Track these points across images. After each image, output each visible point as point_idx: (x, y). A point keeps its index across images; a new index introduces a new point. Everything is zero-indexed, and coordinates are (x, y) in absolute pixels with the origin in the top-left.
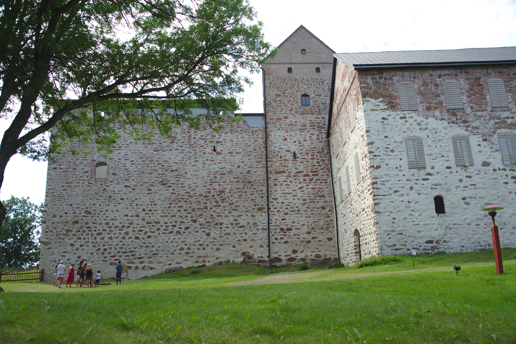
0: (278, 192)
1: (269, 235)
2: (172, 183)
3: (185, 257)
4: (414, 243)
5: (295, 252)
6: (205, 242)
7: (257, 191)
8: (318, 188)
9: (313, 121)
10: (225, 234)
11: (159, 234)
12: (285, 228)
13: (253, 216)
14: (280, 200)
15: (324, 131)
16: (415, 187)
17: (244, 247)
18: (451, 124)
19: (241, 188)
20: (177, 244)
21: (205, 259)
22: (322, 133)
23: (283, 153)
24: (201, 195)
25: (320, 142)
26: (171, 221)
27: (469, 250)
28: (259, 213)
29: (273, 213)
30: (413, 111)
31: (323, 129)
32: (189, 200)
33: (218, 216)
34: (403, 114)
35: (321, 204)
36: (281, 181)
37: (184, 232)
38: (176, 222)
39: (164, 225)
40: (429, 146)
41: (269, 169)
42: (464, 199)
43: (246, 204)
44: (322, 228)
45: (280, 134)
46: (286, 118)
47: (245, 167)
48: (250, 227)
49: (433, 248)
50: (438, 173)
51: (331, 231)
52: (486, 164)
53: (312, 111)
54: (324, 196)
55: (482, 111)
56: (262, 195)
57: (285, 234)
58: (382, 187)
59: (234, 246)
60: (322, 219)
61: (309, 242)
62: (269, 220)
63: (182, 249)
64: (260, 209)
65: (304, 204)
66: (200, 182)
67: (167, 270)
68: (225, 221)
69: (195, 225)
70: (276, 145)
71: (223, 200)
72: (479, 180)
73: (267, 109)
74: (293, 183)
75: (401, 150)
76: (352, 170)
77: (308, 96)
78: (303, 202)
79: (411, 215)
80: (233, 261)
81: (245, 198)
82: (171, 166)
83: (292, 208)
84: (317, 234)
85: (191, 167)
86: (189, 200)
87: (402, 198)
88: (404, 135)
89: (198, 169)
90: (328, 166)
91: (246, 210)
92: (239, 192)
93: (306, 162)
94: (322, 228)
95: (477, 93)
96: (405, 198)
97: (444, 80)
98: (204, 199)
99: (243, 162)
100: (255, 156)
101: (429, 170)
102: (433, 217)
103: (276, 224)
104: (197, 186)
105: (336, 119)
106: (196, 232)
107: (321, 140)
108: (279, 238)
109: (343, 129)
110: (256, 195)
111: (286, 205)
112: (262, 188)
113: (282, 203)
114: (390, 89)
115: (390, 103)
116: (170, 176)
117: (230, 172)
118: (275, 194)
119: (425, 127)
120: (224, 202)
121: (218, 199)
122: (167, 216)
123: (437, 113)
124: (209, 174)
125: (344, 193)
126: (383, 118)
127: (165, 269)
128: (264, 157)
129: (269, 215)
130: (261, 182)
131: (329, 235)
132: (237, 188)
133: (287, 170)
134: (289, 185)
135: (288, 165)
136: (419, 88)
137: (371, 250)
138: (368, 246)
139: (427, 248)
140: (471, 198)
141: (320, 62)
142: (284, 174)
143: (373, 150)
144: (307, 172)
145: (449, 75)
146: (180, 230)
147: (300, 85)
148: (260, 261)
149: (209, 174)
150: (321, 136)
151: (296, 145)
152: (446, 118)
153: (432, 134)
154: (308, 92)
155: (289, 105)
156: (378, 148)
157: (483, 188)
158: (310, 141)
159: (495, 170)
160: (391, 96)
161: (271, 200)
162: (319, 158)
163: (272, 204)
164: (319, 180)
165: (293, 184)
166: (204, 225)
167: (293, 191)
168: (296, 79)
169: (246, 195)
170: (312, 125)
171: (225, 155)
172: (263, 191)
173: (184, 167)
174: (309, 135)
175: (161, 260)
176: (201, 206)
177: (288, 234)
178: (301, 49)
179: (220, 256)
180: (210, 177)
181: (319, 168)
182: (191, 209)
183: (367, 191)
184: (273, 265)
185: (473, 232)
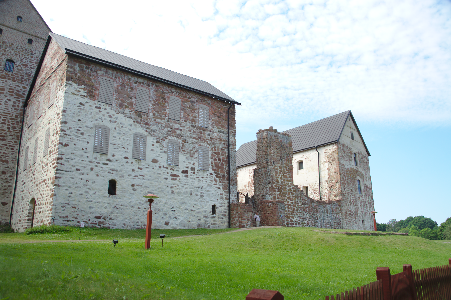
4: (85, 217)
9: (13, 88)
15: (22, 100)
16: (95, 168)
18: (136, 123)
22: (19, 101)
25: (15, 109)
27: (129, 228)
30: (108, 104)
31: (21, 98)
40: (115, 137)
42: (133, 185)
49: (100, 223)
50: (117, 160)
51: (8, 196)
52: (155, 161)
54: (7, 162)
55: (161, 119)
58: (66, 163)
75: (90, 135)
77: (14, 62)
79: (87, 192)
87: (81, 177)
88: (96, 122)
90: (18, 134)
96: (85, 177)
97: (138, 87)
102: (105, 197)
105: (37, 92)
107: (16, 108)
109: (42, 103)
114: (93, 81)
115: (90, 92)
119: (115, 120)
123: (127, 111)
125: (29, 162)
126: (81, 103)
136: (118, 87)
137: (44, 219)
138: (41, 214)
140: (138, 186)
145: (143, 83)
147: (8, 49)
152: (133, 117)
153: (119, 127)
156: (70, 128)
157: (149, 180)
159: (160, 167)
160: (92, 86)
162: (11, 124)
164: (6, 145)
170: (11, 91)
174: (5, 100)
181: (9, 134)
183: (51, 164)
185: (134, 214)
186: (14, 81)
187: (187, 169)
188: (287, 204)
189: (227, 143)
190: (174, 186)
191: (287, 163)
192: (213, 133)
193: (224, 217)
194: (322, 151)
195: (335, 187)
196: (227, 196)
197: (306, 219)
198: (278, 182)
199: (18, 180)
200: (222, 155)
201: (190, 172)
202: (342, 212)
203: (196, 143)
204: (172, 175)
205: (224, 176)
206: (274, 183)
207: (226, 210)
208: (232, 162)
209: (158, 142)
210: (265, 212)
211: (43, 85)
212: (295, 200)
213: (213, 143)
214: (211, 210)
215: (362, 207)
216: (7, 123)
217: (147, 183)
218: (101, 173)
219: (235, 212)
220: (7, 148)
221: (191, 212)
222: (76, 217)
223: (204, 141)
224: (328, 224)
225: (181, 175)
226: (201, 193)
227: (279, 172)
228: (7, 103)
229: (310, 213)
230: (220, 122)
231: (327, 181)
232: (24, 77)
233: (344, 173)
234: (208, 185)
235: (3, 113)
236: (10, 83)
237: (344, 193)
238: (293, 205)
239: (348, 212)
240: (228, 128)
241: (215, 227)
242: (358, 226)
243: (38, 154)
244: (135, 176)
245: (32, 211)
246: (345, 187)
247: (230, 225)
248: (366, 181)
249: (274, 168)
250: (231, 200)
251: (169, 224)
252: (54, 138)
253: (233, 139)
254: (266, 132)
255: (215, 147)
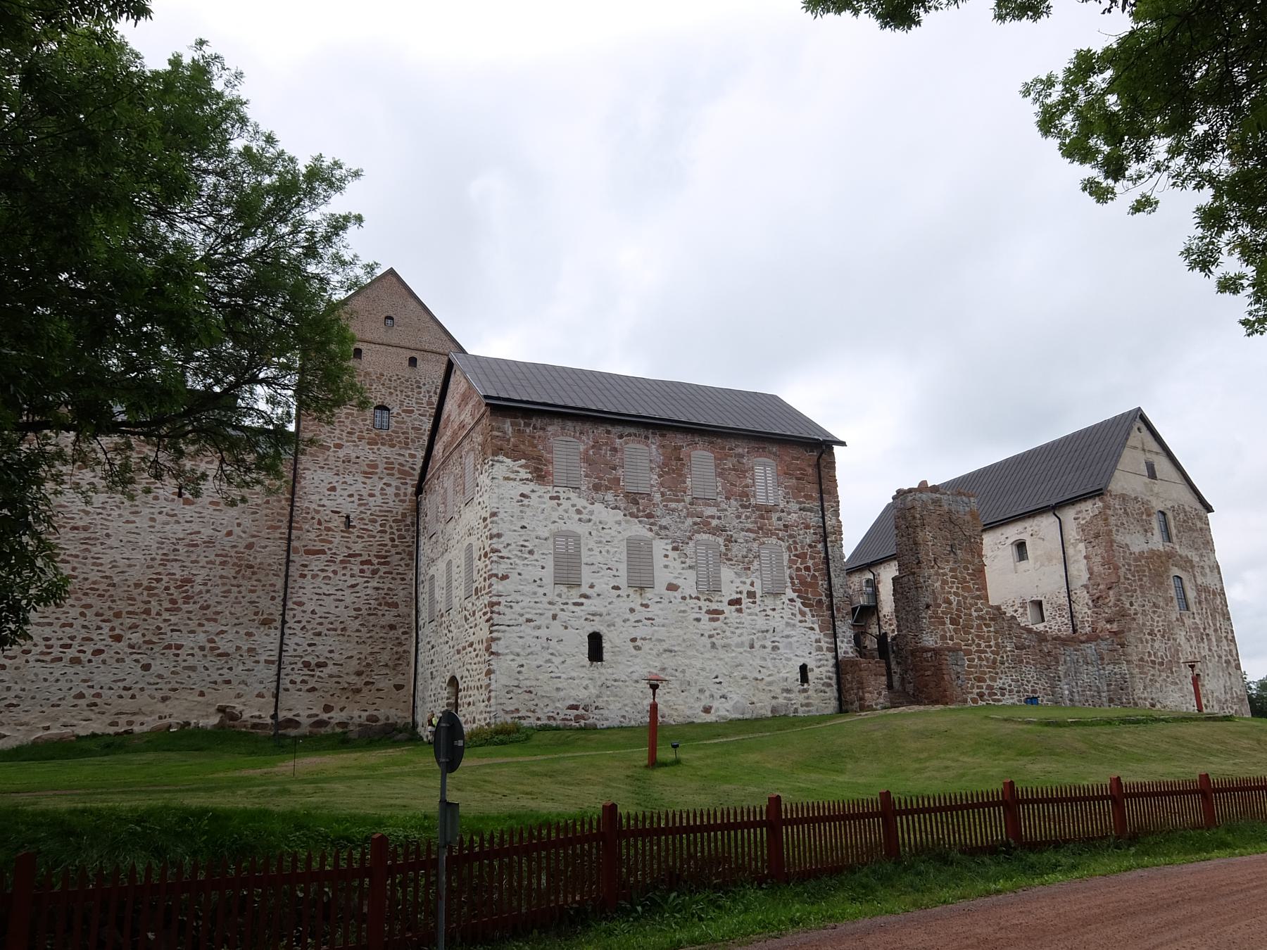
0: (305, 590)
1: (278, 674)
2: (71, 555)
3: (87, 714)
4: (549, 709)
5: (328, 709)
6: (136, 683)
7: (264, 586)
8: (386, 587)
9: (392, 460)
10: (185, 668)
11: (27, 661)
12: (313, 663)
13: (249, 634)
14: (309, 607)
15: (413, 481)
16: (561, 614)
17: (226, 697)
18: (628, 518)
19: (230, 576)
20: (69, 685)
21: (133, 718)
22: (406, 484)
23: (325, 514)
24: (137, 585)
25: (400, 501)
26: (60, 634)
27: (633, 723)
28: (262, 629)
29: (291, 632)
32: (109, 593)
33: (172, 631)
35: (389, 618)
36: (316, 569)
37: (90, 661)
38: (72, 638)
39: (42, 643)
40: (591, 550)
41: (294, 544)
42: (633, 640)
43: (238, 610)
44: (386, 665)
45: (323, 477)
46: (339, 446)
47: (243, 535)
48: (241, 656)
49: (577, 718)
50: (599, 595)
52: (672, 587)
53: (391, 440)
54: (396, 605)
55: (678, 501)
56: (274, 594)
58: (507, 611)
59: (202, 694)
61: (358, 691)
62: (282, 643)
63: (81, 696)
64: (265, 623)
65: (356, 618)
66: (140, 556)
67: (39, 740)
68: (187, 641)
69: (116, 646)
70: (313, 497)
71: (187, 599)
72: (660, 612)
73: (302, 424)
74: (339, 576)
75: (545, 552)
76: (458, 570)
77: (389, 410)
78: (354, 613)
79: (549, 661)
80: (197, 724)
81: (236, 598)
82: (72, 518)
83: (332, 623)
85: (121, 524)
86: (109, 593)
87: (537, 633)
88: (552, 527)
89: (136, 531)
90: (410, 549)
91: (236, 621)
92: (224, 584)
93: (370, 536)
94: (386, 665)
95: (673, 470)
96: (543, 633)
97: (626, 443)
98: (145, 593)
99: (239, 525)
100: (266, 516)
101: (585, 589)
102: (583, 666)
103: (295, 653)
104: (130, 566)
105: (438, 469)
106: (118, 661)
107: (402, 498)
108: (298, 681)
109: (450, 492)
110: (259, 593)
112: (274, 580)
113: (313, 612)
114: (540, 447)
115: (537, 470)
116: (69, 540)
117: (209, 542)
118: (300, 594)
119: (588, 517)
120: (188, 603)
121: (176, 594)
122: (50, 624)
123: (609, 496)
124: (163, 543)
125: (438, 607)
126: (522, 495)
127: (33, 738)
128: (286, 520)
129: (283, 634)
130: (275, 567)
131: (399, 680)
132: (222, 577)
133: (329, 549)
134: (330, 578)
136: (587, 451)
137: (478, 717)
138: (471, 708)
139: (568, 717)
140: (644, 639)
141: (418, 346)
143: (500, 547)
145: (635, 435)
146: (81, 655)
147: (374, 386)
148: (255, 726)
149: (163, 543)
152: (622, 506)
153: (597, 530)
154: (388, 401)
155: (347, 422)
156: (508, 545)
157: (663, 626)
159: (684, 598)
160: (539, 459)
161: (290, 605)
163: (291, 613)
164: (392, 573)
165: (337, 577)
166: (139, 648)
168: (367, 374)
169: (240, 592)
170: (389, 467)
171: (203, 508)
173: (106, 523)
174: (381, 485)
175: (25, 718)
176: (136, 607)
177: (318, 674)
178: (386, 314)
179: (167, 711)
180: (163, 549)
181: (393, 551)
182: (111, 613)
183: (481, 613)
184: (282, 734)
185: (641, 695)
187: (739, 596)
188: (976, 652)
189: (821, 530)
190: (714, 632)
191: (969, 557)
192: (789, 513)
193: (827, 690)
194: (1069, 514)
195: (1107, 600)
196: (831, 643)
198: (950, 603)
200: (812, 558)
201: (745, 601)
202: (1130, 658)
203: (754, 540)
204: (708, 612)
205: (820, 601)
206: (939, 606)
208: (835, 571)
209: (675, 549)
210: (922, 672)
211: (448, 456)
212: (996, 639)
213: (791, 536)
214: (799, 676)
215: (1194, 642)
216: (389, 531)
217: (662, 633)
218: (573, 622)
220: (393, 579)
221: (754, 683)
223: (770, 533)
224: (1090, 690)
226: (773, 642)
227: (950, 580)
229: (1038, 666)
230: (803, 490)
231: (1085, 586)
232: (410, 435)
233: (1129, 565)
234: (788, 624)
235: (380, 511)
236: (386, 450)
237: (1132, 612)
238: (991, 652)
239: (1146, 658)
240: (822, 499)
241: (809, 711)
242: (1181, 689)
243: (454, 592)
244: (637, 621)
245: (452, 701)
246: (1133, 600)
247: (843, 707)
248: (1204, 575)
249: (937, 574)
250: (839, 651)
251: (713, 711)
252: (480, 564)
253: (834, 522)
255: (795, 542)
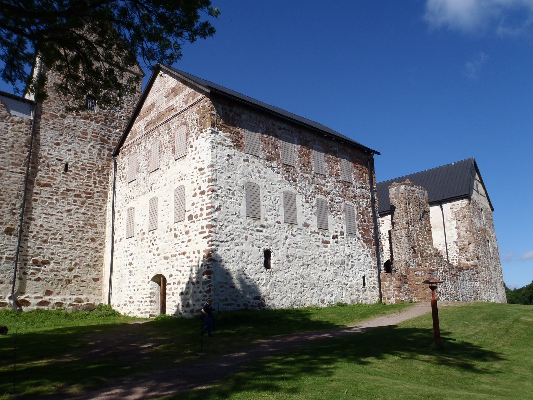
5: (48, 293)
22: (105, 148)
25: (101, 158)
30: (255, 156)
31: (107, 144)
34: (247, 157)
51: (99, 270)
54: (95, 226)
55: (308, 173)
57: (39, 268)
60: (90, 254)
61: (69, 281)
65: (70, 232)
78: (69, 229)
84: (81, 272)
93: (81, 179)
97: (283, 134)
111: (46, 230)
113: (41, 226)
123: (274, 164)
126: (228, 156)
133: (55, 184)
134: (53, 204)
135: (56, 178)
139: (254, 304)
142: (49, 188)
144: (80, 192)
145: (286, 129)
150: (103, 152)
151: (71, 155)
152: (282, 172)
158: (88, 154)
162: (97, 178)
164: (94, 205)
167: (58, 212)
172: (15, 205)
174: (89, 146)
186: (97, 122)
194: (447, 206)
197: (449, 289)
199: (115, 249)
200: (367, 216)
204: (323, 242)
207: (375, 282)
209: (307, 202)
219: (387, 284)
222: (236, 299)
223: (349, 199)
224: (468, 294)
225: (332, 241)
228: (91, 151)
231: (456, 242)
235: (88, 163)
254: (404, 186)
